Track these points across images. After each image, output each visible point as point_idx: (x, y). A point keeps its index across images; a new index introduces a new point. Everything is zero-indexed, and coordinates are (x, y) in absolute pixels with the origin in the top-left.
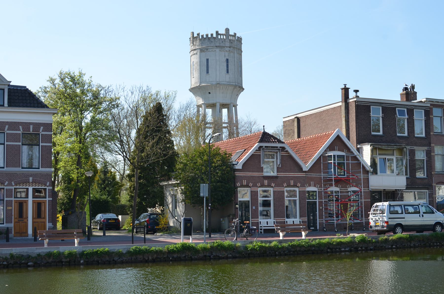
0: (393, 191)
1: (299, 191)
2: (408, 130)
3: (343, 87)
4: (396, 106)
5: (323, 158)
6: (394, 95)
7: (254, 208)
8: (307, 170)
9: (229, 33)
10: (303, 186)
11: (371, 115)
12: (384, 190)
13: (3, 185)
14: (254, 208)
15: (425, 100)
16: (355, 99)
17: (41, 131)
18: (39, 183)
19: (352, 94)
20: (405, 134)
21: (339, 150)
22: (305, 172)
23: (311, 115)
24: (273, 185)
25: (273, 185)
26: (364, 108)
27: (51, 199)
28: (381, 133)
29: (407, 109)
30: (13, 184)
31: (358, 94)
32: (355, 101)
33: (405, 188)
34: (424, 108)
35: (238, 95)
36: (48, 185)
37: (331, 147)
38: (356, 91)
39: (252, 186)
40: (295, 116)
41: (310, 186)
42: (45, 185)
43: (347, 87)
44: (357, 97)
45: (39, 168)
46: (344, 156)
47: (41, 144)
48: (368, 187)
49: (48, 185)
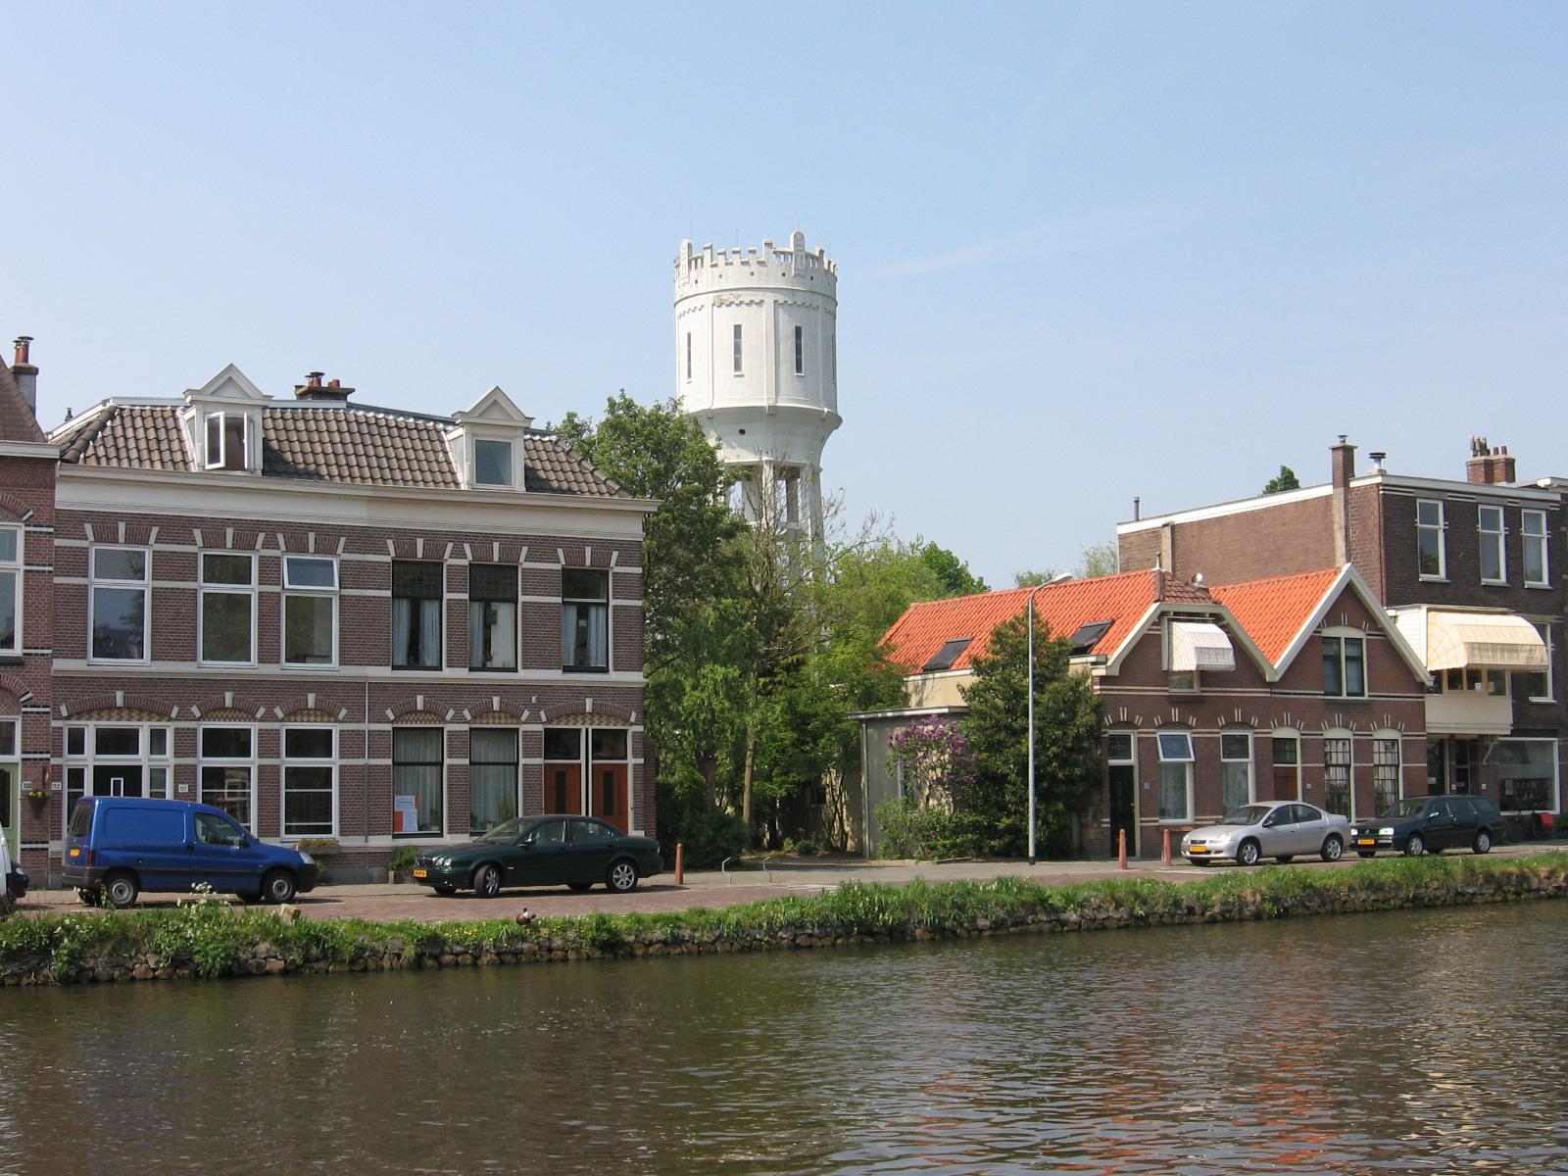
0: (1472, 741)
1: (1256, 739)
2: (1507, 567)
3: (1337, 443)
4: (1417, 493)
5: (1315, 643)
6: (1453, 469)
7: (1147, 786)
8: (1277, 679)
9: (803, 246)
10: (1264, 724)
11: (1418, 525)
12: (1453, 735)
13: (515, 721)
14: (1147, 786)
15: (1548, 482)
16: (1379, 480)
17: (446, 556)
18: (610, 716)
19: (1364, 466)
20: (1437, 573)
21: (1351, 625)
22: (1271, 685)
23: (1221, 520)
24: (1192, 721)
25: (1192, 721)
26: (1400, 506)
27: (642, 761)
28: (1442, 574)
29: (1506, 508)
30: (65, 713)
31: (1384, 464)
32: (1378, 485)
33: (1509, 733)
34: (1547, 505)
35: (823, 440)
36: (632, 719)
37: (1331, 617)
38: (1378, 457)
39: (1142, 727)
40: (1164, 521)
41: (1332, 726)
42: (626, 721)
43: (1349, 442)
44: (1382, 473)
45: (515, 670)
46: (1361, 640)
47: (521, 599)
48: (1423, 728)
49: (632, 719)
